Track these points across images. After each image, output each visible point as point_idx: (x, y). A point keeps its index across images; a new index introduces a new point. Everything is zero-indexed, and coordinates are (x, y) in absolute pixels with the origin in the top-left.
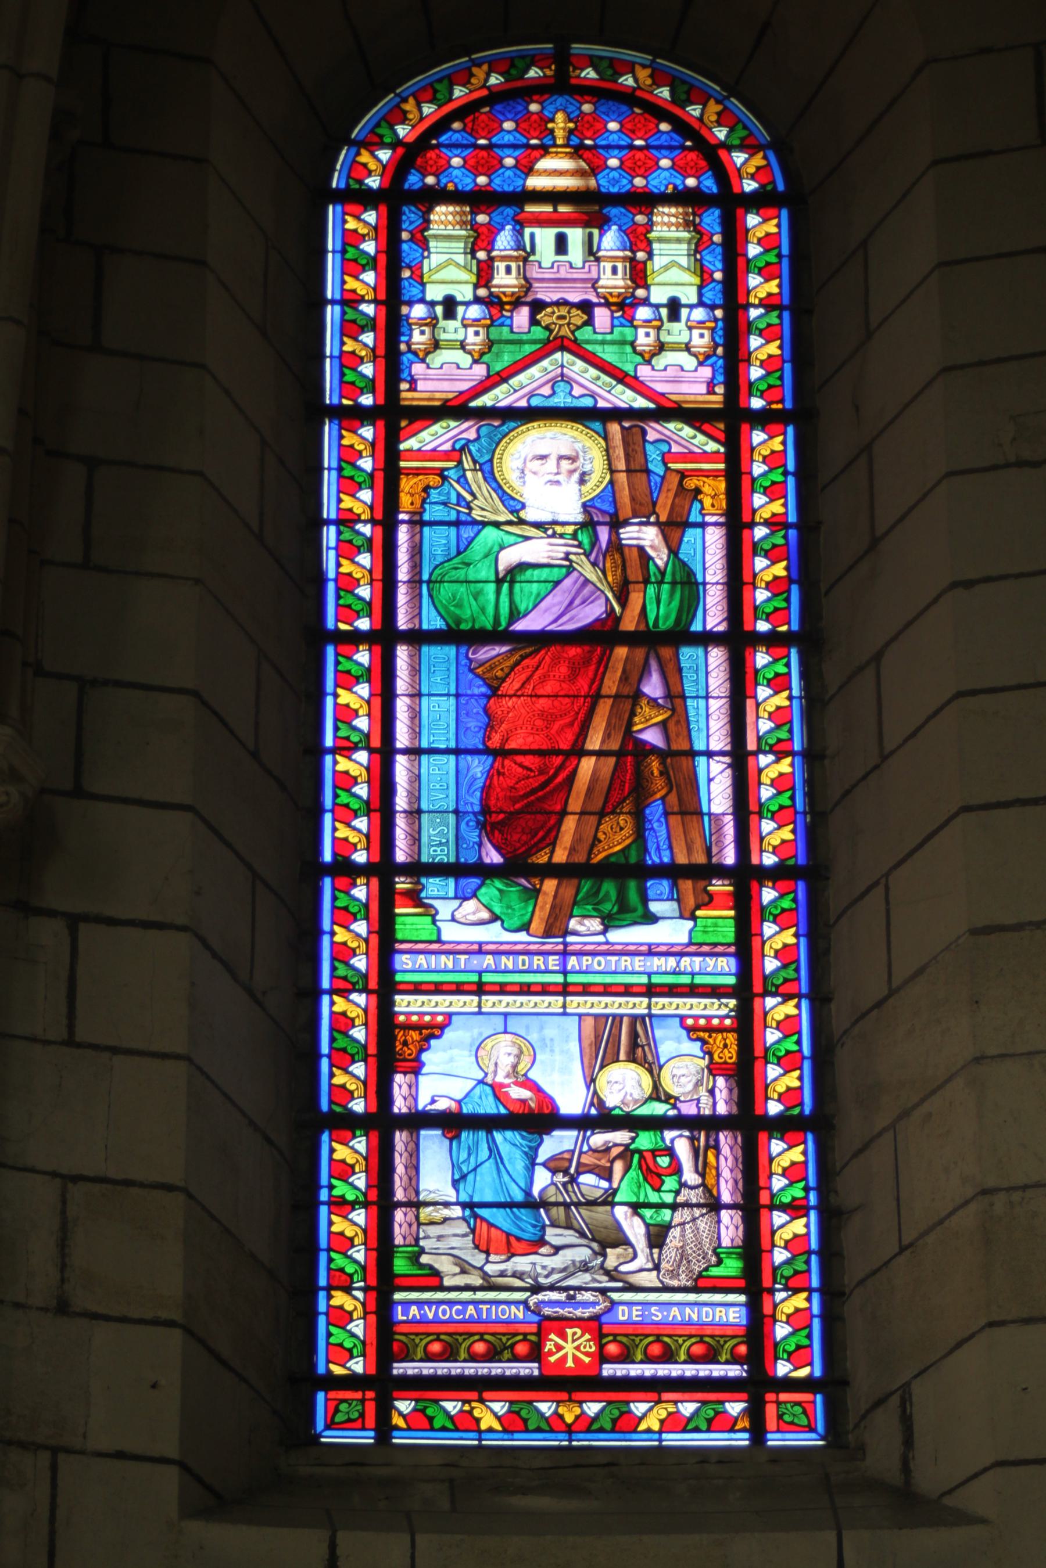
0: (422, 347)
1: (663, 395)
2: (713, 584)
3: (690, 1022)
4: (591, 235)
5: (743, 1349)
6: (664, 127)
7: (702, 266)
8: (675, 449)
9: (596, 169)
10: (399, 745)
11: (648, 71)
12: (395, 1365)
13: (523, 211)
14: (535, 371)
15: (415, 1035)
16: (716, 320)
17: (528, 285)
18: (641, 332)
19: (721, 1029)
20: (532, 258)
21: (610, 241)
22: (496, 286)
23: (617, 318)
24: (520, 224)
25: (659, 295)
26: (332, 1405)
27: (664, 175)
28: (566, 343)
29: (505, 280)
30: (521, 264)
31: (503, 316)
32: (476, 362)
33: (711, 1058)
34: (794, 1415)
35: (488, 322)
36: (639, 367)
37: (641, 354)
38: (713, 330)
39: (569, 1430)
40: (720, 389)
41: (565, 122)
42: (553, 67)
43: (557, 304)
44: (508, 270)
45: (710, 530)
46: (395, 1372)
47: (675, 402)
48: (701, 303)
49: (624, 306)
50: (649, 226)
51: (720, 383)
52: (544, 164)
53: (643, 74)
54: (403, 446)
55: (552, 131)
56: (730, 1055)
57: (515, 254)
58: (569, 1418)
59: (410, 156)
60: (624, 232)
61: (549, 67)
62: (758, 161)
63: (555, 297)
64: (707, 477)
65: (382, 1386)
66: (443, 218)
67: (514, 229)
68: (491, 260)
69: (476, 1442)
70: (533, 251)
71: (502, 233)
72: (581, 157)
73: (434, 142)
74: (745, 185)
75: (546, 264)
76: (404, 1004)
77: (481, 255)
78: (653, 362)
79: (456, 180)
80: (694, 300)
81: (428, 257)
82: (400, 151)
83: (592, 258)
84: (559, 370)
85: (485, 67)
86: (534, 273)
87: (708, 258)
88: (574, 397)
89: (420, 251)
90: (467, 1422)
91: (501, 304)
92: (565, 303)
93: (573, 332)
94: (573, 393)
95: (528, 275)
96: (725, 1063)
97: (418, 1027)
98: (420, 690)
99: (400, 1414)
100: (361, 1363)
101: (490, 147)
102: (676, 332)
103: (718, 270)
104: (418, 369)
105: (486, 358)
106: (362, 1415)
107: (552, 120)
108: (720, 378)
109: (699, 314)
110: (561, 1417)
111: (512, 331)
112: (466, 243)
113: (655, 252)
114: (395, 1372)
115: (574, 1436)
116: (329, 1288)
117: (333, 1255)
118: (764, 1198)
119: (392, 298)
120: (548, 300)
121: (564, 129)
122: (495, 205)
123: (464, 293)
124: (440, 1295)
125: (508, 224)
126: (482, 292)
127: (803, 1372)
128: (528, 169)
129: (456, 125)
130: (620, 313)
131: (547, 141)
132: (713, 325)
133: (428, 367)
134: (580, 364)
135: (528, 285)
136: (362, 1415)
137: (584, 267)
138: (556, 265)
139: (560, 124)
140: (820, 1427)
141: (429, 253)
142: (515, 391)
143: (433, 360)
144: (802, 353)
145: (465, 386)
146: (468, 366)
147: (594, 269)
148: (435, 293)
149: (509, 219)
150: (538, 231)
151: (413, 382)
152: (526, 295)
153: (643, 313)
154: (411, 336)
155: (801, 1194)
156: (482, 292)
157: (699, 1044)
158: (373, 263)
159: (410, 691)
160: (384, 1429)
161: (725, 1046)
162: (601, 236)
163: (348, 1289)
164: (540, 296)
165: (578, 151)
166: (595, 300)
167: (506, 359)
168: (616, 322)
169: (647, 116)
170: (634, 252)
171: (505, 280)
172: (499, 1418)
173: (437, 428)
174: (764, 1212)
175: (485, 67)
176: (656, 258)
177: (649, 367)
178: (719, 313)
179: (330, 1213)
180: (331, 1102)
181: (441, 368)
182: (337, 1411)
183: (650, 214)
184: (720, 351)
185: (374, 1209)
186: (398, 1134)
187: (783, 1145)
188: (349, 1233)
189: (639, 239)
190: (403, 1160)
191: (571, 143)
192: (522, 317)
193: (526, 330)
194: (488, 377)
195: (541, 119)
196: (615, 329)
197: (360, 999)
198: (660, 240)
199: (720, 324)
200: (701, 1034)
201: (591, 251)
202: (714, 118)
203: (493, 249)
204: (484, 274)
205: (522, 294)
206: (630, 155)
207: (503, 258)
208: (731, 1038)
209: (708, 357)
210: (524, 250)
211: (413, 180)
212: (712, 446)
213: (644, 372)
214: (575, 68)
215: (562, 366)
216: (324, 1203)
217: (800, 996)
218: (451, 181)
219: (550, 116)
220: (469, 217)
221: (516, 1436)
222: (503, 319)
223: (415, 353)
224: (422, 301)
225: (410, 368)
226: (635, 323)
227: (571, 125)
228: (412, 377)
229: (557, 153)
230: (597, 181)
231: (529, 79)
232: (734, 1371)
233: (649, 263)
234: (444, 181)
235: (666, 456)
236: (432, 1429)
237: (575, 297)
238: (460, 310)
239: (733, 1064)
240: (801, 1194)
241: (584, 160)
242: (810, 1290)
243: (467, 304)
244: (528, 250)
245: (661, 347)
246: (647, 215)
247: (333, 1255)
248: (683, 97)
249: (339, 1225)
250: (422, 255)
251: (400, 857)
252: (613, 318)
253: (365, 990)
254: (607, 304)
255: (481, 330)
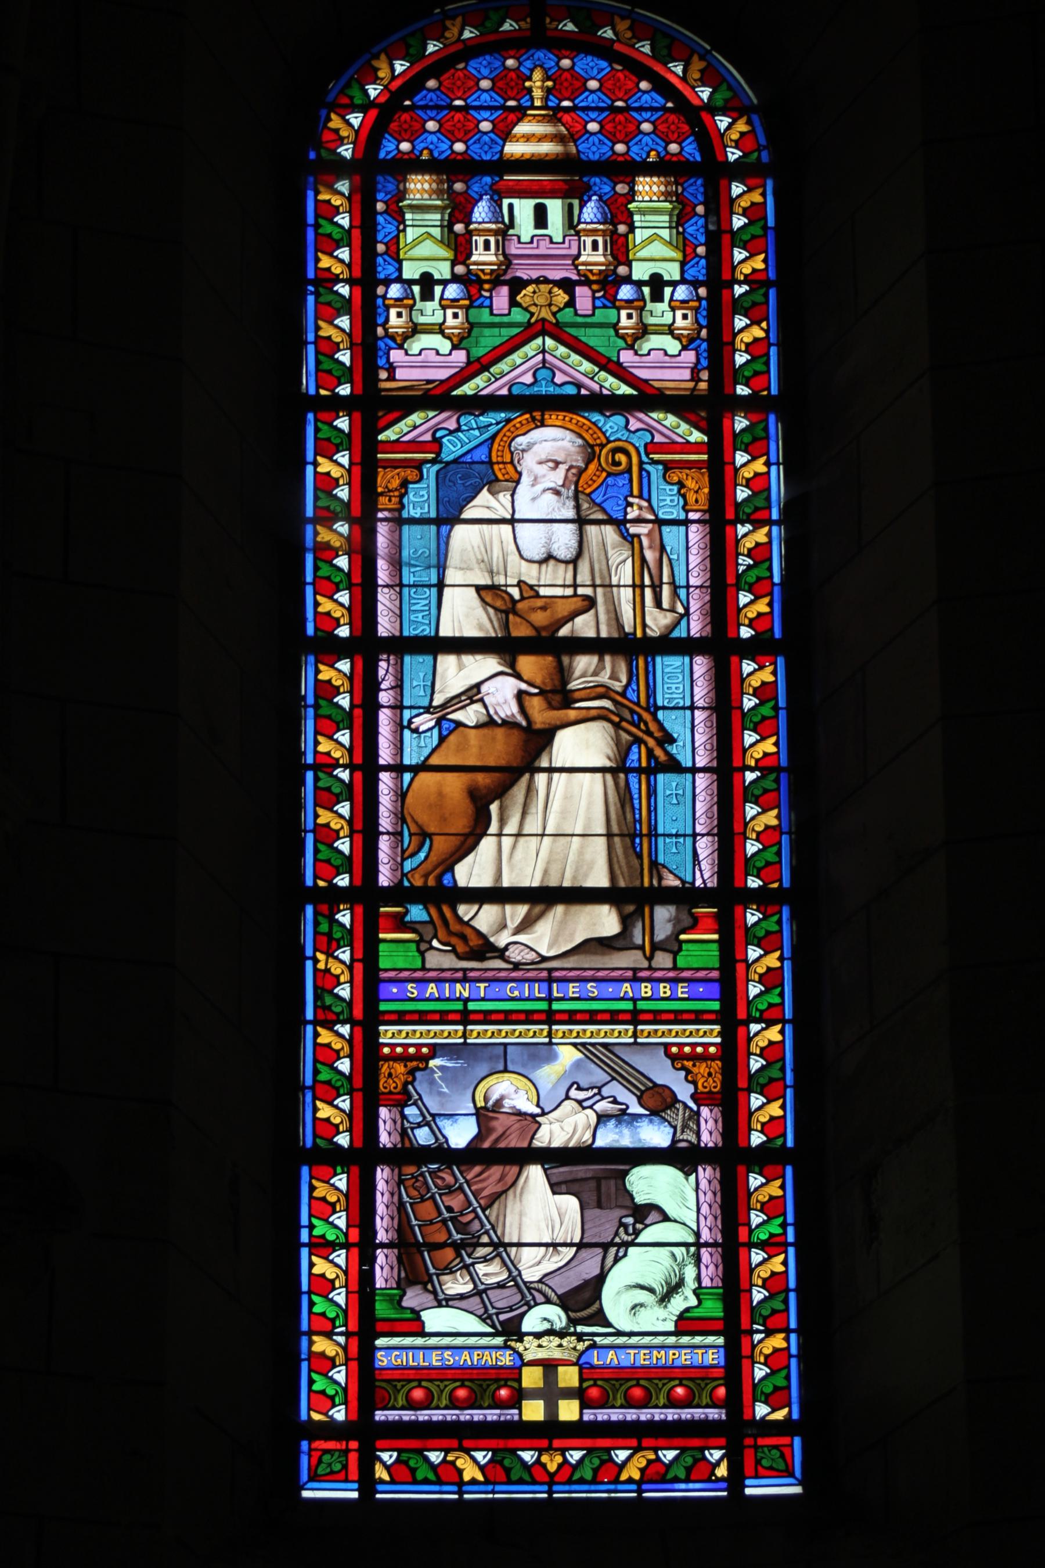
0: (400, 331)
1: (646, 381)
2: (697, 587)
3: (674, 1050)
4: (571, 207)
5: (722, 1391)
6: (644, 85)
7: (685, 239)
8: (658, 438)
9: (575, 135)
10: (381, 762)
11: (627, 23)
12: (377, 1412)
13: (501, 179)
14: (516, 357)
15: (400, 1068)
16: (699, 299)
17: (508, 261)
18: (624, 313)
19: (705, 1057)
20: (511, 232)
21: (590, 211)
22: (476, 263)
23: (598, 298)
24: (497, 195)
25: (641, 271)
26: (316, 1455)
27: (645, 147)
28: (547, 326)
29: (483, 257)
30: (500, 238)
31: (481, 296)
32: (455, 347)
33: (696, 1088)
34: (773, 1460)
35: (467, 302)
36: (622, 352)
37: (623, 337)
38: (696, 310)
39: (551, 1480)
40: (705, 375)
41: (543, 81)
42: (528, 20)
43: (537, 281)
44: (487, 246)
45: (693, 528)
46: (377, 1418)
47: (658, 389)
48: (683, 281)
49: (607, 284)
50: (631, 196)
51: (704, 368)
52: (522, 129)
53: (623, 25)
54: (381, 437)
55: (530, 90)
56: (715, 1084)
57: (493, 226)
58: (552, 1467)
59: (386, 116)
60: (605, 202)
61: (524, 20)
62: (742, 126)
63: (535, 275)
64: (690, 469)
65: (364, 1434)
66: (419, 186)
67: (492, 198)
68: (469, 233)
69: (456, 1496)
70: (512, 224)
71: (479, 204)
72: (560, 120)
73: (407, 103)
74: (729, 155)
75: (525, 238)
76: (389, 1035)
77: (459, 228)
78: (406, 346)
79: (431, 147)
80: (677, 277)
81: (404, 230)
82: (373, 113)
83: (572, 232)
84: (540, 357)
85: (459, 20)
86: (513, 249)
87: (690, 230)
88: (556, 384)
89: (396, 224)
90: (448, 1475)
91: (480, 282)
92: (546, 281)
93: (554, 314)
94: (556, 380)
95: (507, 252)
96: (390, 1093)
97: (405, 1058)
98: (402, 701)
99: (384, 1464)
100: (343, 1412)
101: (466, 109)
102: (660, 313)
103: (701, 245)
104: (396, 355)
105: (464, 344)
106: (345, 1467)
107: (530, 79)
108: (704, 363)
109: (682, 292)
110: (544, 1466)
111: (492, 314)
112: (671, 215)
113: (637, 224)
114: (377, 1418)
115: (555, 1488)
116: (310, 1333)
117: (315, 1298)
118: (743, 1234)
119: (367, 279)
120: (525, 277)
121: (542, 88)
122: (473, 176)
123: (442, 270)
124: (419, 1341)
125: (486, 194)
126: (460, 269)
127: (780, 1415)
128: (504, 133)
129: (432, 84)
130: (601, 294)
131: (525, 102)
132: (696, 304)
133: (407, 354)
134: (562, 350)
135: (508, 261)
136: (345, 1467)
137: (563, 242)
138: (535, 239)
139: (537, 84)
140: (798, 1472)
141: (405, 226)
142: (497, 380)
143: (410, 345)
144: (792, 338)
145: (443, 374)
146: (447, 352)
147: (575, 245)
148: (411, 271)
149: (487, 188)
150: (515, 202)
151: (391, 369)
152: (505, 272)
153: (626, 292)
154: (387, 320)
155: (779, 1231)
156: (460, 269)
157: (683, 1073)
158: (346, 238)
159: (392, 702)
160: (367, 1484)
161: (710, 1074)
162: (582, 207)
163: (329, 1335)
164: (519, 274)
165: (554, 115)
166: (575, 277)
167: (487, 341)
168: (598, 303)
169: (627, 73)
170: (615, 226)
171: (483, 257)
172: (482, 1468)
173: (416, 418)
174: (742, 1251)
175: (459, 20)
176: (637, 231)
177: (631, 352)
178: (702, 291)
179: (310, 1254)
180: (315, 1136)
181: (420, 354)
182: (320, 1461)
183: (632, 184)
184: (704, 333)
185: (355, 1251)
186: (379, 1170)
187: (761, 1180)
188: (331, 1275)
189: (619, 215)
190: (707, 1176)
191: (550, 104)
192: (501, 298)
193: (506, 312)
194: (469, 363)
195: (518, 77)
196: (597, 311)
197: (345, 1030)
198: (643, 212)
199: (704, 303)
200: (685, 1063)
201: (571, 223)
202: (697, 76)
203: (471, 223)
204: (460, 248)
205: (501, 272)
206: (664, 118)
207: (480, 232)
208: (717, 1065)
209: (691, 340)
210: (503, 222)
211: (388, 148)
212: (697, 436)
213: (626, 357)
214: (552, 21)
215: (544, 351)
216: (305, 1245)
217: (784, 1021)
218: (427, 148)
219: (528, 73)
220: (446, 186)
221: (498, 1488)
222: (482, 300)
223: (392, 338)
224: (399, 279)
225: (388, 354)
226: (617, 304)
227: (550, 84)
228: (391, 364)
229: (534, 116)
230: (577, 147)
231: (503, 32)
232: (714, 1414)
233: (630, 236)
234: (420, 146)
235: (649, 446)
236: (415, 1482)
237: (557, 275)
238: (438, 290)
239: (717, 1093)
240: (779, 1231)
241: (563, 125)
242: (787, 1331)
243: (444, 283)
244: (506, 220)
245: (644, 331)
246: (628, 184)
247: (315, 1298)
248: (664, 52)
249: (321, 1267)
250: (398, 228)
251: (384, 881)
252: (594, 298)
253: (350, 1020)
254: (586, 282)
255: (460, 312)
